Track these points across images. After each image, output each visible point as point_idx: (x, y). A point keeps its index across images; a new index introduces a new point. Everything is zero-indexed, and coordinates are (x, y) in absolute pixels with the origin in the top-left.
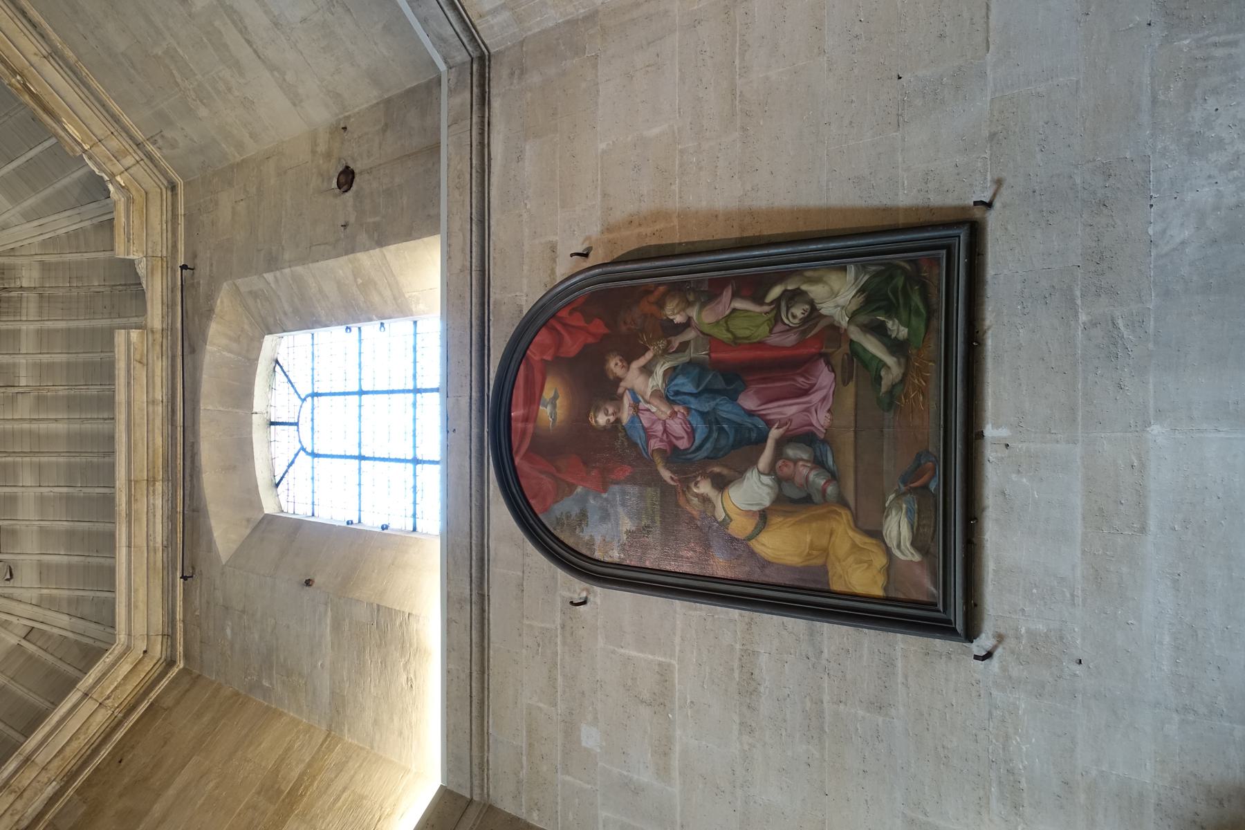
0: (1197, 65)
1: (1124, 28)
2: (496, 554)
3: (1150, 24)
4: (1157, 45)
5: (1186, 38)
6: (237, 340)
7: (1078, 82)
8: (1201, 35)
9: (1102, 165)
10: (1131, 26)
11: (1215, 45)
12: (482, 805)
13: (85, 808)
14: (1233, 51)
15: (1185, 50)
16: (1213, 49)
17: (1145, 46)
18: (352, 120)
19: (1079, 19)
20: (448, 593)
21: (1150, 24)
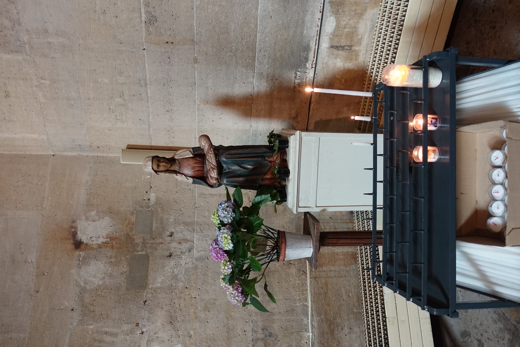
0: (95, 344)
1: (57, 308)
2: (432, 82)
3: (73, 310)
4: (75, 324)
5: (91, 325)
6: (306, 14)
7: (24, 338)
8: (99, 325)
9: (342, 216)
10: (62, 307)
11: (106, 333)
12: (148, 83)
13: (388, 169)
14: (115, 339)
15: (90, 333)
16: (105, 336)
17: (69, 324)
18: (452, 92)
19: (32, 294)
20: (320, 131)
21: (73, 310)
